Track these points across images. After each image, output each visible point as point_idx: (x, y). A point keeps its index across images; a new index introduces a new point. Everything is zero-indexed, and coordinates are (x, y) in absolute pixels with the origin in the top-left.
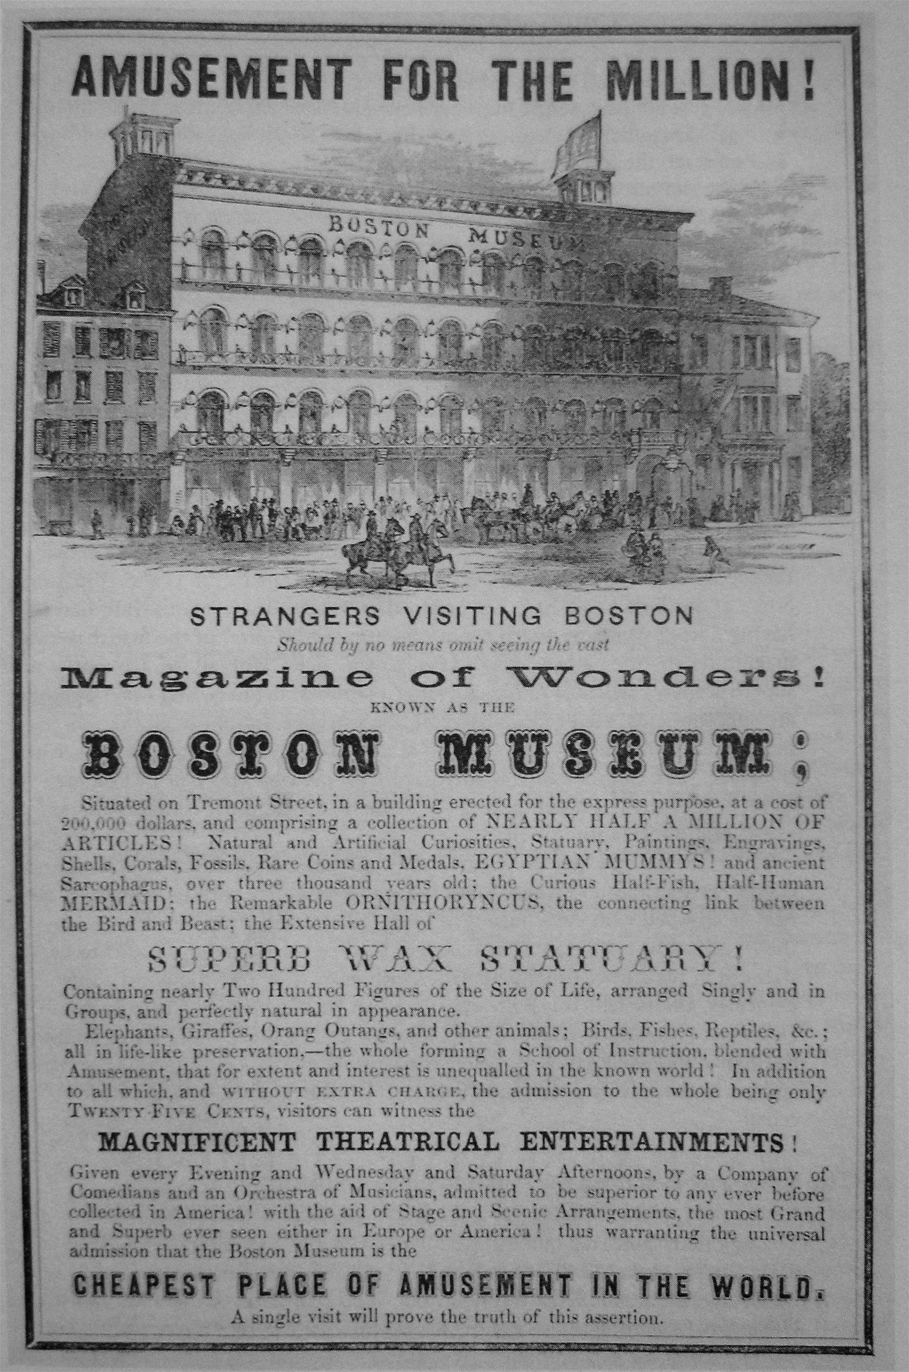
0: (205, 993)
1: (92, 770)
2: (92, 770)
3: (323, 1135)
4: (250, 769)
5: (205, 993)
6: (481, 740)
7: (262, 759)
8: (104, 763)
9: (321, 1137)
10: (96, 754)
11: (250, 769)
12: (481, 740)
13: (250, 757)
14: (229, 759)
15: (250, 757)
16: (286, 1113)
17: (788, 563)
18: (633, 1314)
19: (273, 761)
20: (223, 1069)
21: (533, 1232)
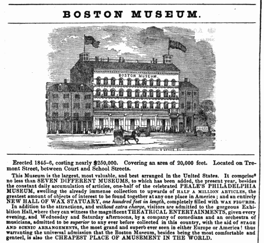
1: (65, 17)
2: (65, 17)
10: (65, 14)
13: (97, 15)
15: (97, 15)
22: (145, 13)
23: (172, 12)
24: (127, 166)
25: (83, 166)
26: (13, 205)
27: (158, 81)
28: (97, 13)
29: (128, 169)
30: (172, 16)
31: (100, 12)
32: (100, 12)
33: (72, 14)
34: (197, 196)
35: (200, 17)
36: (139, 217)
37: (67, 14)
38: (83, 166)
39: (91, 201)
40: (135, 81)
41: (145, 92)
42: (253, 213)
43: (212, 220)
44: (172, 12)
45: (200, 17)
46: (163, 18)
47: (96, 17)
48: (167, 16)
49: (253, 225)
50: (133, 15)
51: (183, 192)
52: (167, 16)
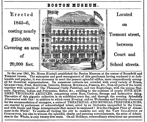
0: (34, 32)
1: (48, 6)
2: (48, 6)
3: (117, 76)
4: (60, 6)
5: (34, 32)
6: (75, 4)
7: (61, 6)
8: (49, 6)
9: (110, 33)
10: (48, 5)
11: (60, 6)
12: (75, 4)
13: (60, 5)
14: (58, 6)
15: (60, 5)
16: (52, 111)
17: (75, 12)
18: (16, 30)
19: (62, 6)
20: (27, 64)
21: (50, 85)
22: (96, 6)
23: (87, 4)
24: (25, 75)
25: (52, 75)
26: (118, 93)
27: (88, 31)
28: (60, 4)
29: (25, 77)
30: (87, 6)
31: (61, 4)
32: (61, 4)
33: (51, 5)
34: (102, 84)
35: (98, 6)
36: (23, 105)
37: (49, 5)
38: (52, 75)
39: (38, 94)
40: (70, 32)
41: (88, 39)
42: (76, 94)
43: (114, 95)
44: (87, 4)
45: (98, 6)
46: (84, 7)
47: (60, 7)
48: (85, 6)
49: (6, 107)
50: (69, 5)
51: (84, 85)
52: (85, 6)
